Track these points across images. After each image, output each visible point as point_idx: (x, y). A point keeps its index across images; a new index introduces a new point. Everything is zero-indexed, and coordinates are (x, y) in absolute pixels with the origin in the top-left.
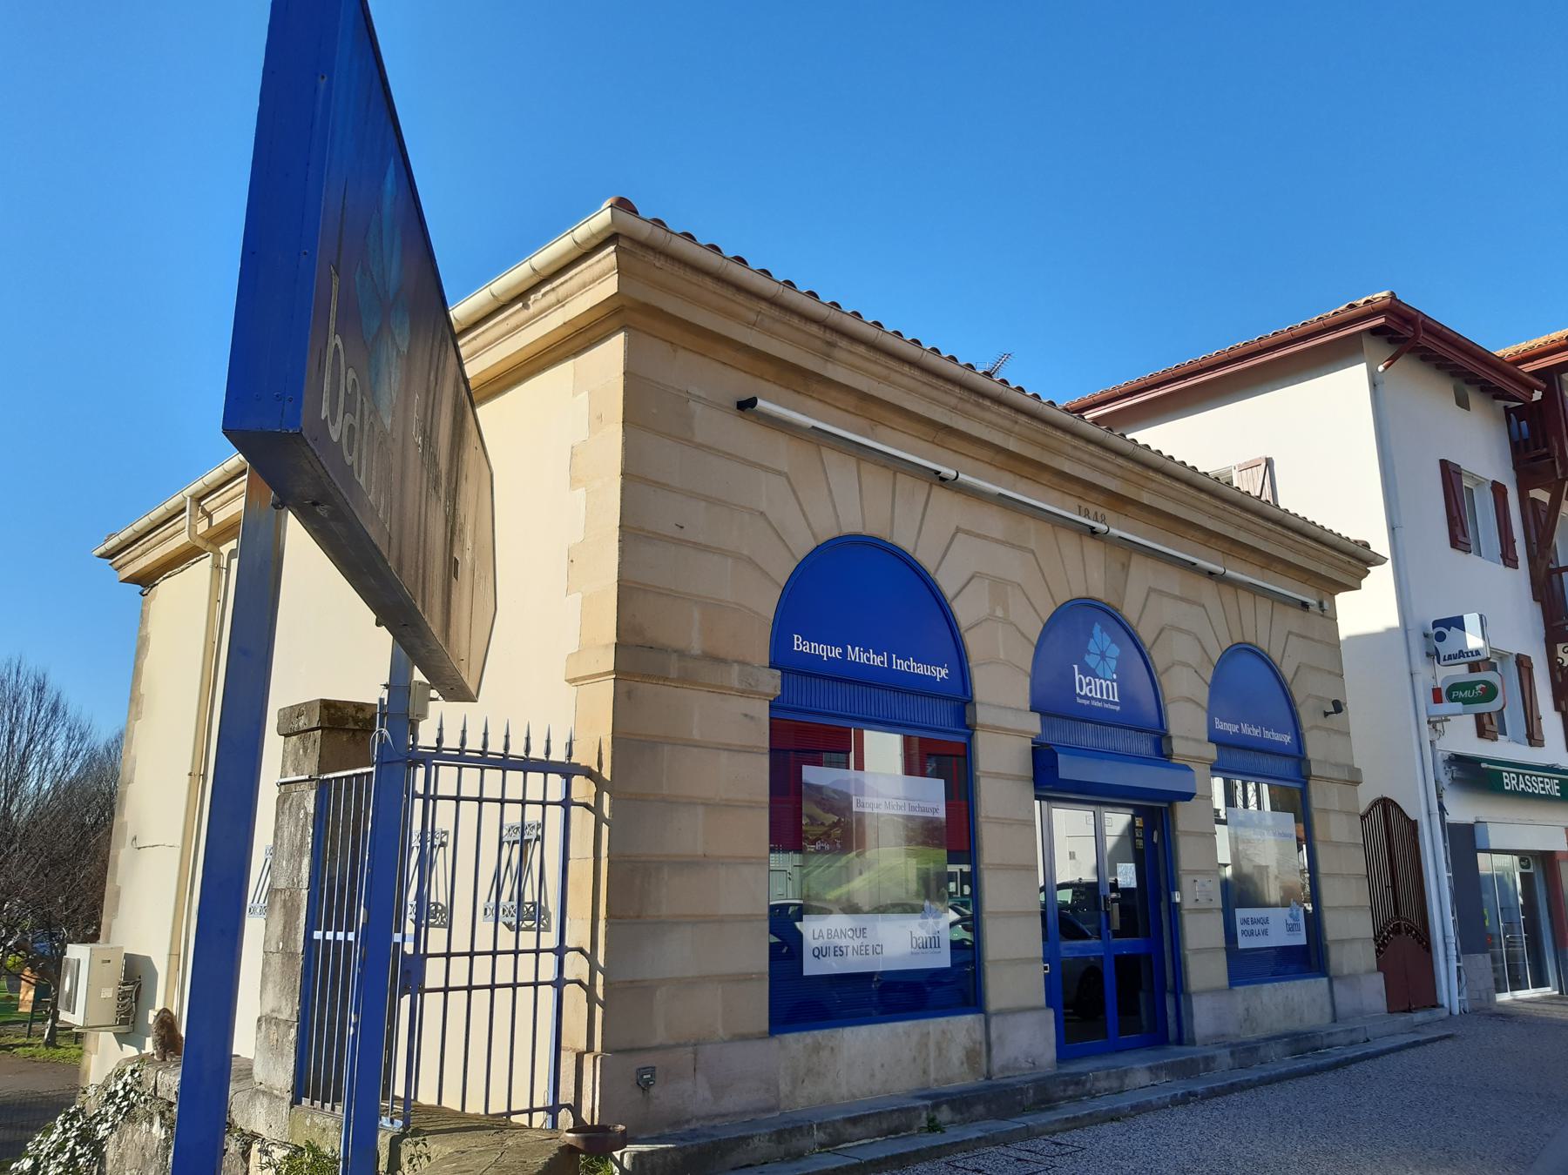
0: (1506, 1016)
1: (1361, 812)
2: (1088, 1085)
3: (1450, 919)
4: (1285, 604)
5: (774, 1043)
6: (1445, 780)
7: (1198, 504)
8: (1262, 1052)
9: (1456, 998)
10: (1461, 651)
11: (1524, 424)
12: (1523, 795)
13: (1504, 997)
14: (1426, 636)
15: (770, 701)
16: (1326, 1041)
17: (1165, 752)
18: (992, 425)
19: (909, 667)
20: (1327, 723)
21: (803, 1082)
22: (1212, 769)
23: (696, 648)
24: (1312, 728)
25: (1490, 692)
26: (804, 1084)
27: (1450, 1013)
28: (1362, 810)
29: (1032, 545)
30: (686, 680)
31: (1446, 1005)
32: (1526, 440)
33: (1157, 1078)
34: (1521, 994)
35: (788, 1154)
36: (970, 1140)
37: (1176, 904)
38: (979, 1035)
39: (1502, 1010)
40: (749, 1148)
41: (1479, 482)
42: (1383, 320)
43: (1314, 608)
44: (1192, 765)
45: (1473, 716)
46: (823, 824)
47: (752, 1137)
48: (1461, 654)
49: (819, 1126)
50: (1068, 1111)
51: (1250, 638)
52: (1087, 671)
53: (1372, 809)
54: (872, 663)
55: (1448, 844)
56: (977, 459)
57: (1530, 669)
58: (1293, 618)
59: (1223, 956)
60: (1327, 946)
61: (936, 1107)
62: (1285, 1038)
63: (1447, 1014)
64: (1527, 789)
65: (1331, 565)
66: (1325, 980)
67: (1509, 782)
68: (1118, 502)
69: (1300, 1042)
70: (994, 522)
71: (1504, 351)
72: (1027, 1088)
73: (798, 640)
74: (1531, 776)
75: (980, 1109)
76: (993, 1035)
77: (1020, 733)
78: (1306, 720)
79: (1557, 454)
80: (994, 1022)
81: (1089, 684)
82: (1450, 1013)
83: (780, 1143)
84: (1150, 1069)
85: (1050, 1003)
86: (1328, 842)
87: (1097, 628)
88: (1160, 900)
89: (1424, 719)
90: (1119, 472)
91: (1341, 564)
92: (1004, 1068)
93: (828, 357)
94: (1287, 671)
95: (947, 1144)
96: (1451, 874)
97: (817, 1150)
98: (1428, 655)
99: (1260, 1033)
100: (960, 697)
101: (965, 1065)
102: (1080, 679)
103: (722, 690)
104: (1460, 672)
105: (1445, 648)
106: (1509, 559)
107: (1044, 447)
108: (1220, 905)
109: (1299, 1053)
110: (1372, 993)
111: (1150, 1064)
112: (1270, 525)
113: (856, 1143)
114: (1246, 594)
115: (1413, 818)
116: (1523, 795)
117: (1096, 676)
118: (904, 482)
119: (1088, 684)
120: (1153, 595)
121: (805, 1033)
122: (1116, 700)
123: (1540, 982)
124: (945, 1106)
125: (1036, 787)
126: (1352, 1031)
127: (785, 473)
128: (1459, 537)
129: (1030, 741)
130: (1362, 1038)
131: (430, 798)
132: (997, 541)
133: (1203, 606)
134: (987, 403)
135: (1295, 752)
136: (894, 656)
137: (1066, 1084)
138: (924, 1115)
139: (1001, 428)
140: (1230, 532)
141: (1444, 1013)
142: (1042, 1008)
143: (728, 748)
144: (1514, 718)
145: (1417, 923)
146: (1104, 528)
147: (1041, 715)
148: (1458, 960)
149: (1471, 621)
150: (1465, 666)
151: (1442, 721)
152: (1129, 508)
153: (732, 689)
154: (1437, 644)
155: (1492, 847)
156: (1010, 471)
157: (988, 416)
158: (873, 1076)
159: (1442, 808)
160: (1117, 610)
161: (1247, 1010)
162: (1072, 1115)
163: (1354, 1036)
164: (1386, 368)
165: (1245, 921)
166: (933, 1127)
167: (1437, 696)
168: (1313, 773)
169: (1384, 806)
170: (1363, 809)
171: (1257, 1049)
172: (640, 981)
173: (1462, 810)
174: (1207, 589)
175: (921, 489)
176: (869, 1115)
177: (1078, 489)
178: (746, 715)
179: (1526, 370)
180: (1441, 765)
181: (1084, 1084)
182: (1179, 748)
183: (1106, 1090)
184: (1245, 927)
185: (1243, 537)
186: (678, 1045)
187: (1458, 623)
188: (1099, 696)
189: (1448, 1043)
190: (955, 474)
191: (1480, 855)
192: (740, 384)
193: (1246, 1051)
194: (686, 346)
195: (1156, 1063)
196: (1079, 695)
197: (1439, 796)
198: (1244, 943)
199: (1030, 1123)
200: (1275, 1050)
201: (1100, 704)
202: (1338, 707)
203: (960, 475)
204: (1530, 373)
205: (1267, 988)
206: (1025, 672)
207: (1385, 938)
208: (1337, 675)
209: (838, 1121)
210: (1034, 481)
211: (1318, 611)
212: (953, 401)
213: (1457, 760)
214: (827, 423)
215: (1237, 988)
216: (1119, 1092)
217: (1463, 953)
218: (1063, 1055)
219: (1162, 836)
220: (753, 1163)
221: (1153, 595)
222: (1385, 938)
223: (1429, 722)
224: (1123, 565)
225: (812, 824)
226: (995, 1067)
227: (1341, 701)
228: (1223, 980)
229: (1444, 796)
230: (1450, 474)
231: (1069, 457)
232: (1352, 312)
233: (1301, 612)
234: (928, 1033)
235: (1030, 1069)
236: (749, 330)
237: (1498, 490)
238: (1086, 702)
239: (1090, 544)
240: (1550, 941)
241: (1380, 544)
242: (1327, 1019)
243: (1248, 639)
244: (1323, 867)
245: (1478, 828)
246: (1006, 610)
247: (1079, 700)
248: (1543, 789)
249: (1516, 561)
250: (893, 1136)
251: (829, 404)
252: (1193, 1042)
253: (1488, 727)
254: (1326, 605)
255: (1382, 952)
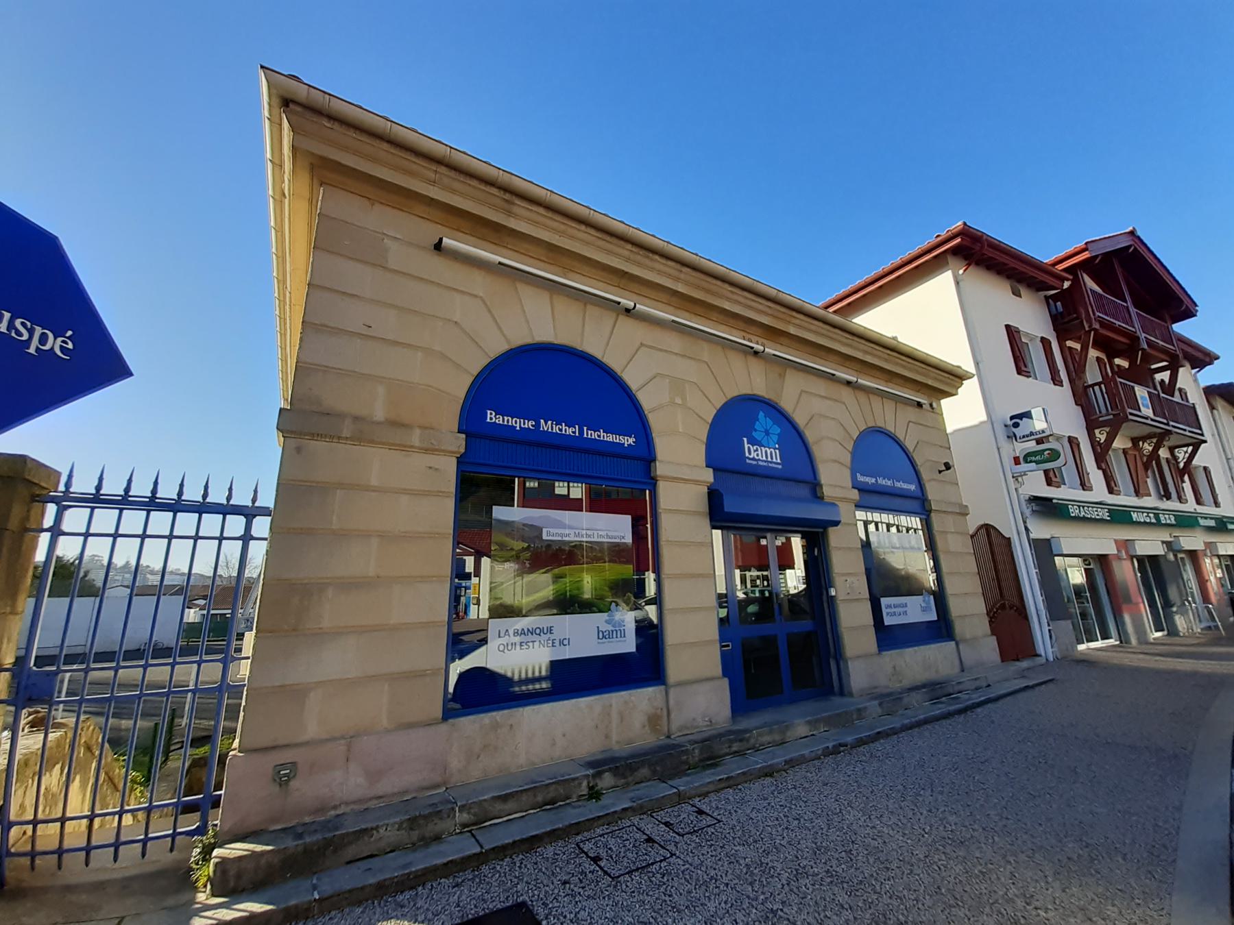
0: (1085, 662)
1: (971, 533)
2: (752, 741)
3: (1040, 599)
4: (906, 404)
5: (444, 727)
6: (1028, 512)
7: (834, 336)
8: (906, 700)
9: (1050, 650)
10: (1031, 432)
11: (1059, 304)
12: (1084, 519)
13: (1081, 647)
14: (1006, 426)
15: (457, 458)
16: (957, 688)
17: (819, 495)
18: (660, 272)
19: (599, 436)
20: (941, 477)
21: (479, 757)
22: (856, 506)
23: (380, 414)
24: (930, 481)
25: (1054, 455)
26: (480, 759)
27: (1047, 660)
28: (971, 532)
29: (706, 358)
30: (360, 439)
31: (1043, 654)
32: (1061, 313)
33: (816, 729)
34: (1093, 645)
35: (422, 839)
36: (615, 812)
37: (832, 597)
38: (660, 703)
39: (1083, 657)
40: (372, 839)
41: (1032, 338)
42: (959, 240)
43: (926, 407)
44: (837, 503)
45: (1042, 472)
46: (512, 549)
47: (377, 828)
48: (1032, 434)
49: (462, 808)
50: (733, 767)
51: (880, 424)
52: (753, 442)
53: (978, 530)
54: (564, 432)
55: (1033, 552)
56: (658, 301)
57: (1078, 445)
58: (912, 413)
59: (872, 631)
60: (952, 621)
61: (598, 775)
62: (924, 688)
63: (1044, 660)
64: (1086, 516)
65: (936, 379)
66: (953, 643)
67: (1074, 511)
68: (773, 333)
69: (935, 689)
70: (673, 341)
71: (1047, 259)
72: (693, 749)
73: (491, 414)
74: (1088, 507)
75: (644, 772)
76: (672, 702)
77: (696, 482)
78: (925, 476)
79: (1083, 316)
80: (672, 692)
81: (757, 450)
82: (1047, 660)
83: (411, 829)
84: (809, 723)
85: (726, 673)
86: (948, 552)
87: (761, 414)
88: (822, 594)
89: (1009, 476)
90: (769, 311)
91: (943, 379)
92: (681, 729)
93: (509, 213)
94: (910, 445)
95: (588, 820)
96: (1037, 570)
97: (458, 831)
98: (1008, 437)
99: (906, 683)
100: (645, 456)
101: (647, 728)
102: (749, 448)
103: (405, 448)
104: (1031, 445)
105: (1019, 432)
106: (1056, 381)
107: (708, 291)
108: (867, 596)
109: (935, 699)
110: (989, 649)
111: (809, 718)
112: (889, 352)
113: (505, 819)
114: (876, 397)
115: (1007, 536)
116: (1084, 519)
117: (761, 445)
118: (592, 310)
119: (755, 451)
120: (803, 394)
121: (482, 715)
122: (779, 461)
123: (1105, 636)
124: (607, 773)
125: (711, 520)
126: (976, 679)
127: (481, 297)
128: (1022, 365)
129: (706, 488)
130: (985, 684)
131: (56, 532)
132: (676, 354)
133: (844, 403)
134: (657, 257)
135: (920, 494)
136: (585, 428)
137: (731, 741)
138: (585, 784)
139: (669, 276)
140: (859, 355)
141: (1042, 660)
142: (719, 678)
143: (405, 492)
144: (1069, 472)
145: (1016, 601)
146: (761, 348)
147: (714, 470)
148: (1049, 625)
149: (1037, 413)
150: (1034, 442)
151: (1021, 476)
152: (782, 340)
153: (412, 447)
154: (1014, 430)
155: (1065, 552)
156: (688, 311)
157: (657, 266)
158: (554, 744)
159: (1027, 529)
160: (777, 403)
161: (894, 667)
162: (726, 776)
163: (978, 683)
164: (965, 271)
165: (889, 606)
166: (594, 794)
167: (1017, 461)
168: (933, 508)
169: (987, 529)
170: (972, 531)
171: (900, 699)
172: (297, 684)
173: (1041, 530)
174: (846, 393)
175: (608, 318)
176: (521, 791)
177: (741, 325)
178: (430, 468)
179: (1060, 269)
180: (1024, 503)
181: (748, 740)
182: (827, 491)
183: (769, 743)
184: (889, 610)
185: (869, 359)
186: (333, 739)
187: (1027, 415)
188: (764, 458)
189: (1051, 686)
190: (633, 304)
191: (1056, 558)
192: (430, 231)
193: (890, 699)
194: (383, 201)
195: (815, 717)
196: (748, 458)
197: (1025, 522)
198: (888, 621)
199: (682, 788)
200: (915, 699)
201: (765, 464)
202: (948, 466)
203: (637, 305)
204: (1061, 270)
205: (909, 651)
206: (702, 441)
207: (995, 613)
208: (947, 448)
209: (485, 800)
210: (707, 318)
211: (929, 409)
212: (626, 253)
213: (1035, 499)
214: (517, 262)
215: (884, 653)
216: (781, 744)
217: (1052, 620)
218: (739, 707)
219: (819, 550)
220: (375, 853)
221: (803, 394)
222: (995, 613)
223: (1013, 477)
224: (780, 375)
225: (502, 550)
226: (674, 727)
227: (951, 464)
228: (873, 647)
229: (1028, 521)
230: (1012, 333)
231: (728, 299)
232: (939, 239)
233: (917, 409)
234: (611, 706)
235: (708, 726)
236: (432, 187)
237: (1045, 342)
238: (754, 463)
239: (753, 361)
240: (1110, 609)
241: (968, 366)
242: (957, 670)
243: (879, 424)
244: (945, 568)
245: (1053, 541)
246: (684, 399)
247: (748, 461)
248: (1098, 515)
249: (1062, 382)
250: (548, 807)
251: (522, 253)
252: (851, 694)
253: (1054, 479)
254: (935, 405)
255: (993, 622)
